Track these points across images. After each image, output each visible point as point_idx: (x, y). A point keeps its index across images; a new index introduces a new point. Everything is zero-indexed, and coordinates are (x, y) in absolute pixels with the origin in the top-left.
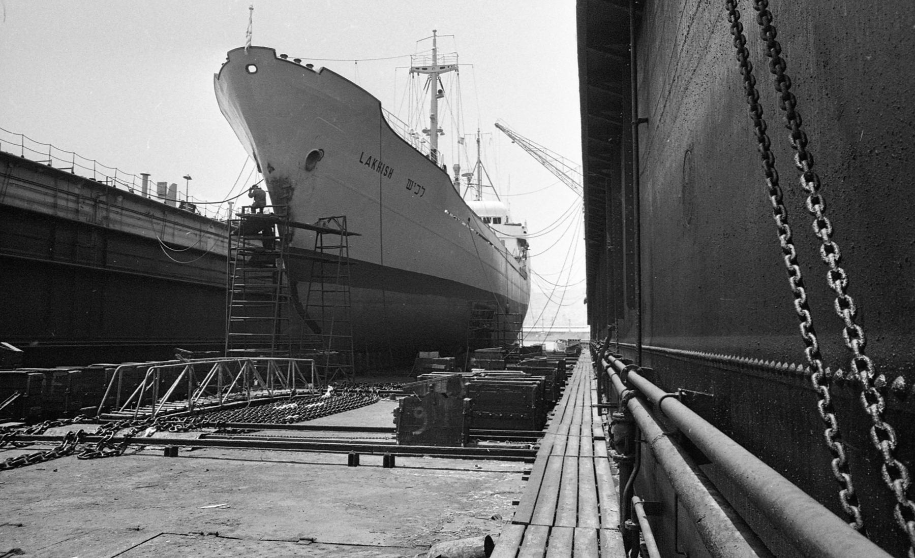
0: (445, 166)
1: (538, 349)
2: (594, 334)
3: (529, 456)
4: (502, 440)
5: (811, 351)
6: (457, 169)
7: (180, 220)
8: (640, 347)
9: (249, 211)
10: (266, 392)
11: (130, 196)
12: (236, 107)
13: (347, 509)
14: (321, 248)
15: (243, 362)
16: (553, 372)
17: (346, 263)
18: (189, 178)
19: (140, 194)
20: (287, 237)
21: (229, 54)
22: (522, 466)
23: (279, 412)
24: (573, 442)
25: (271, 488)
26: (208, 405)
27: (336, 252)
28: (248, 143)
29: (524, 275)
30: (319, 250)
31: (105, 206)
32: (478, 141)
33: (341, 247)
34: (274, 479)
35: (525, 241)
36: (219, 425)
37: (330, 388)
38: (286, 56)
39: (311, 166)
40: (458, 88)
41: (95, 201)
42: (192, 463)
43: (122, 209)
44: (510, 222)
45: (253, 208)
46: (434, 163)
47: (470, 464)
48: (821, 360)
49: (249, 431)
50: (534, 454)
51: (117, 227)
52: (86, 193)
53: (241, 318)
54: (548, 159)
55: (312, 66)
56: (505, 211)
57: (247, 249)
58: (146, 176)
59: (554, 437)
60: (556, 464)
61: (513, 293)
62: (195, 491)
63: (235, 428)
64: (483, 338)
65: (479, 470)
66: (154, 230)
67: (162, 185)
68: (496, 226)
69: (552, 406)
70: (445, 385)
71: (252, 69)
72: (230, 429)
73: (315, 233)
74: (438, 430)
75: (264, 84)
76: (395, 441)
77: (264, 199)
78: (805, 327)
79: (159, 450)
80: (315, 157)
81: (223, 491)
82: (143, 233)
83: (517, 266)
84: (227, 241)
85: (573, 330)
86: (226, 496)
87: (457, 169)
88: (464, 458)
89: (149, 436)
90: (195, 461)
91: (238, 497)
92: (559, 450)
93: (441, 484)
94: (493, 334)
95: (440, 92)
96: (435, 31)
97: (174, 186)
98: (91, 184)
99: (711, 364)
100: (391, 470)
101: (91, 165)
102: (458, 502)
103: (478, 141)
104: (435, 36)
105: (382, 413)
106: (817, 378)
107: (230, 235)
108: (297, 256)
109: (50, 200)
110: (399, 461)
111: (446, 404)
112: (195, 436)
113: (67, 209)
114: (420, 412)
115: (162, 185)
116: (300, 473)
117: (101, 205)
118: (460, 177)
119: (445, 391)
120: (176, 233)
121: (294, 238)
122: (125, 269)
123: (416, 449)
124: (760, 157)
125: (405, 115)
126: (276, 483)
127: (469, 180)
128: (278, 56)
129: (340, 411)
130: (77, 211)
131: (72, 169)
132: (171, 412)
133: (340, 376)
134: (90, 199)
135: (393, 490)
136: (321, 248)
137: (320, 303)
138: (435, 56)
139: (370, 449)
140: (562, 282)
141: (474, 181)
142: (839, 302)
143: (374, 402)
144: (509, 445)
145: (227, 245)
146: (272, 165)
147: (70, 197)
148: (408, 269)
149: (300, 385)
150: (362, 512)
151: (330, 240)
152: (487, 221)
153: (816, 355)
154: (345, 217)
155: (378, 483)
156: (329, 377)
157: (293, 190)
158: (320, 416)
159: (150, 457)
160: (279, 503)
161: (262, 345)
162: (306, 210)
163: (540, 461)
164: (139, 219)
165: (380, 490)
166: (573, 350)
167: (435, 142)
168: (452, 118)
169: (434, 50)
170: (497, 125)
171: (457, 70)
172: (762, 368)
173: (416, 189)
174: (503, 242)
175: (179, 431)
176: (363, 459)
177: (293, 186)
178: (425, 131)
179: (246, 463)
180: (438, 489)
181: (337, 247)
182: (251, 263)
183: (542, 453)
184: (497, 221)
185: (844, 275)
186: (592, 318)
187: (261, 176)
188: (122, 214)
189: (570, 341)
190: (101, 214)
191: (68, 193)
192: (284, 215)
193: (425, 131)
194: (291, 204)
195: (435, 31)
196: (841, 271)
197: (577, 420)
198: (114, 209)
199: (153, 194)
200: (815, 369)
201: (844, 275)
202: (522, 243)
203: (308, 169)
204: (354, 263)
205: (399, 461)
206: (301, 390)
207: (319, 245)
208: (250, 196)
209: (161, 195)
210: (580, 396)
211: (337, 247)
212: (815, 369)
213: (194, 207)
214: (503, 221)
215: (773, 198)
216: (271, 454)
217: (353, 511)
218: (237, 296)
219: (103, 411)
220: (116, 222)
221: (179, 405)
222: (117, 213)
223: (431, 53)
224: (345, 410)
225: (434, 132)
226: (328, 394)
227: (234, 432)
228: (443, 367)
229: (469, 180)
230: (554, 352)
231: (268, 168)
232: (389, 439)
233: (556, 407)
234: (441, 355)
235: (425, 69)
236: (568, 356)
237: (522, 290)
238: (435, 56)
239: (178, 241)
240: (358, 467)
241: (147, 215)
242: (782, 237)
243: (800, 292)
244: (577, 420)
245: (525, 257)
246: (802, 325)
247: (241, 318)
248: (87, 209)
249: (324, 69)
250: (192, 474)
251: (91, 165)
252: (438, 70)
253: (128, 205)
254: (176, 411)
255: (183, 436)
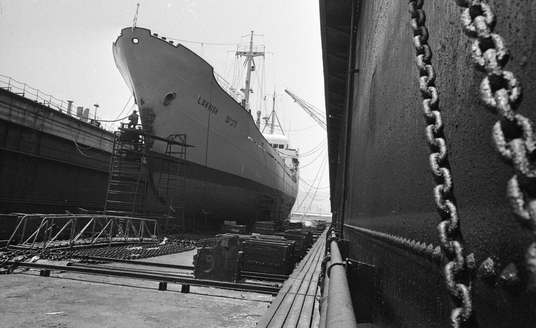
0: (250, 110)
1: (300, 225)
2: (334, 217)
3: (274, 292)
4: (261, 280)
5: (447, 227)
6: (259, 114)
7: (87, 130)
8: (342, 225)
9: (126, 127)
10: (123, 239)
11: (59, 114)
12: (124, 62)
13: (145, 321)
14: (170, 153)
15: (109, 219)
16: (303, 239)
17: (184, 164)
18: (97, 106)
19: (66, 113)
20: (149, 145)
21: (122, 31)
22: (269, 297)
23: (128, 251)
24: (305, 285)
25: (101, 302)
26: (83, 244)
27: (178, 156)
28: (131, 87)
29: (295, 180)
30: (168, 154)
31: (42, 118)
32: (274, 99)
33: (182, 153)
34: (107, 296)
35: (297, 160)
36: (84, 257)
37: (166, 239)
38: (157, 35)
39: (167, 103)
40: (263, 65)
41: (36, 114)
42: (56, 281)
43: (53, 121)
44: (289, 148)
45: (129, 125)
46: (244, 108)
47: (238, 294)
48: (461, 242)
49: (104, 263)
50: (278, 291)
51: (49, 131)
52: (31, 109)
53: (116, 192)
54: (315, 113)
55: (172, 42)
56: (286, 141)
57: (124, 150)
58: (70, 102)
59: (294, 281)
60: (289, 299)
61: (287, 190)
62: (48, 301)
63: (91, 261)
64: (266, 215)
65: (243, 298)
66: (72, 136)
67: (80, 109)
68: (280, 150)
69: (299, 260)
70: (227, 242)
71: (136, 41)
72: (90, 260)
73: (166, 143)
74: (225, 270)
75: (140, 49)
76: (193, 275)
77: (137, 119)
78: (442, 192)
79: (38, 271)
80: (170, 97)
81: (68, 302)
82: (59, 135)
83: (291, 174)
84: (113, 144)
85: (322, 215)
86: (68, 307)
87: (259, 114)
88: (235, 290)
89: (34, 262)
90: (60, 280)
91: (75, 307)
92: (294, 290)
93: (215, 307)
94: (272, 213)
95: (253, 67)
96: (252, 32)
97: (88, 110)
98: (34, 104)
99: (374, 240)
100: (186, 295)
101: (35, 92)
102: (222, 321)
103: (274, 99)
104: (252, 34)
105: (187, 258)
106: (453, 270)
107: (115, 141)
108: (154, 157)
109: (6, 111)
110: (192, 288)
111: (227, 254)
112: (64, 263)
113: (17, 118)
114: (210, 258)
115: (80, 109)
116: (125, 293)
117: (40, 117)
118: (261, 118)
119: (227, 246)
120: (86, 137)
121: (154, 145)
122: (49, 157)
123: (203, 282)
124: (409, 15)
125: (229, 76)
126: (106, 299)
127: (267, 121)
128: (152, 34)
129: (167, 254)
130: (24, 120)
131: (24, 93)
132: (57, 247)
133: (175, 232)
134: (33, 113)
135: (181, 309)
136: (170, 153)
137: (166, 187)
138: (251, 46)
139: (174, 281)
140: (316, 185)
141: (270, 122)
142: (503, 129)
143: (191, 250)
144: (265, 283)
145: (112, 147)
146: (144, 100)
147: (20, 111)
148: (223, 170)
149: (147, 235)
150: (155, 323)
151: (175, 148)
152: (275, 146)
153: (454, 234)
154: (185, 136)
155: (174, 304)
156: (167, 232)
157: (155, 116)
158: (153, 256)
159: (30, 276)
160: (101, 313)
161: (127, 210)
162: (162, 130)
163: (280, 296)
164: (63, 128)
165: (174, 309)
166: (321, 226)
167: (247, 96)
168: (259, 84)
169: (251, 43)
170: (286, 91)
171: (263, 55)
172: (405, 247)
173: (232, 122)
174: (284, 160)
175: (55, 260)
176: (170, 285)
177: (155, 114)
178: (242, 90)
179: (92, 284)
180: (212, 310)
181: (179, 153)
182: (126, 159)
183: (283, 291)
184: (282, 147)
185: (513, 82)
186: (334, 209)
187: (137, 106)
188: (52, 124)
189: (319, 221)
190: (39, 122)
191: (20, 108)
192: (148, 130)
193: (242, 90)
194: (153, 124)
195: (252, 32)
196: (508, 75)
197: (312, 270)
198: (47, 120)
199: (74, 113)
200: (451, 256)
201: (513, 82)
202: (295, 161)
203: (165, 104)
204: (188, 163)
205: (192, 288)
206: (147, 239)
207: (168, 151)
208: (129, 119)
209: (79, 114)
210: (318, 255)
211: (179, 153)
212: (451, 256)
213: (99, 124)
214: (285, 147)
215: (417, 38)
216: (112, 279)
217: (150, 322)
218: (114, 178)
219: (11, 243)
220: (48, 128)
221: (64, 243)
222: (50, 123)
223: (249, 44)
224: (171, 253)
225: (247, 91)
226: (164, 242)
227: (93, 263)
228: (238, 231)
229: (267, 121)
230: (310, 227)
231: (141, 102)
232: (190, 273)
233: (302, 261)
234: (238, 224)
235: (245, 53)
236: (318, 230)
237: (293, 189)
238: (251, 46)
239: (86, 143)
240: (165, 291)
241: (68, 126)
242: (423, 78)
243: (439, 144)
244: (312, 270)
245: (296, 169)
246: (437, 189)
247: (116, 192)
248: (30, 119)
249: (179, 45)
250: (51, 289)
251: (35, 92)
252: (253, 54)
253: (56, 118)
254: (60, 246)
255: (57, 264)
